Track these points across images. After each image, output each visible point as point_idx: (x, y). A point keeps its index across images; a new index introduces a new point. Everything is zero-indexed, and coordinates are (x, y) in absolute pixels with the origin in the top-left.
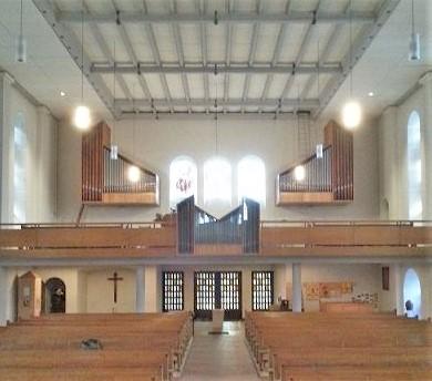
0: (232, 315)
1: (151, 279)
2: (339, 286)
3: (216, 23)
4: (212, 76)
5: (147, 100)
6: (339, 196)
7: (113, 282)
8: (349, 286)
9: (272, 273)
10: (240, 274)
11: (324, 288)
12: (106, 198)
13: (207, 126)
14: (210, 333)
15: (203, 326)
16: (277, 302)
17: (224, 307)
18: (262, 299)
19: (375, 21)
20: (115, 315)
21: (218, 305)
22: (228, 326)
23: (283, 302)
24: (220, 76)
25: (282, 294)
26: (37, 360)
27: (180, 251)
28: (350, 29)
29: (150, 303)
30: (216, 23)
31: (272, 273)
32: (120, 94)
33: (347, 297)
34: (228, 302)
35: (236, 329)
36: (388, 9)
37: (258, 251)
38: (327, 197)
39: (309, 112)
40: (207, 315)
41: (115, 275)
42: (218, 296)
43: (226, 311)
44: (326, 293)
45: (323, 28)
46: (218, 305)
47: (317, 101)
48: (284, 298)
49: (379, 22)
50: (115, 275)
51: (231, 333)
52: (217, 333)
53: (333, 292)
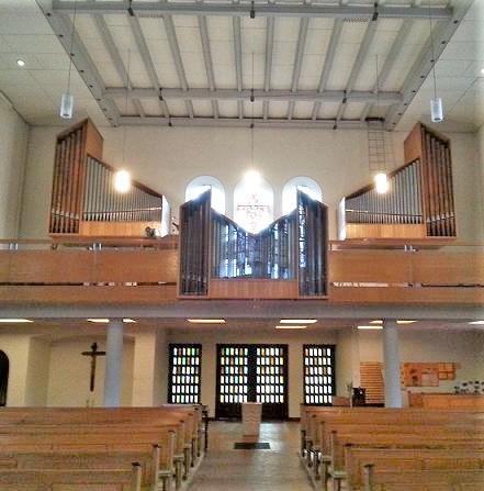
0: (275, 413)
1: (146, 352)
2: (434, 368)
3: (253, 16)
4: (246, 20)
5: (154, 89)
6: (433, 231)
7: (90, 358)
8: (450, 368)
9: (333, 348)
10: (285, 348)
11: (413, 371)
12: (86, 229)
13: (242, 136)
14: (238, 446)
15: (227, 432)
16: (349, 395)
17: (260, 400)
18: (317, 387)
19: (402, 100)
20: (89, 412)
21: (252, 396)
22: (268, 431)
23: (356, 390)
24: (260, 20)
25: (354, 378)
26: (110, 450)
27: (183, 291)
28: (421, 29)
29: (142, 390)
30: (253, 16)
31: (333, 348)
32: (112, 77)
33: (446, 386)
34: (269, 392)
35: (282, 438)
36: (405, 102)
37: (325, 291)
38: (417, 232)
39: (382, 119)
40: (229, 412)
41: (94, 347)
42: (252, 384)
43: (266, 406)
44: (415, 378)
45: (388, 27)
46: (252, 396)
47: (398, 94)
48: (357, 385)
49: (456, 17)
50: (94, 347)
51: (274, 446)
52: (249, 445)
53: (425, 377)
